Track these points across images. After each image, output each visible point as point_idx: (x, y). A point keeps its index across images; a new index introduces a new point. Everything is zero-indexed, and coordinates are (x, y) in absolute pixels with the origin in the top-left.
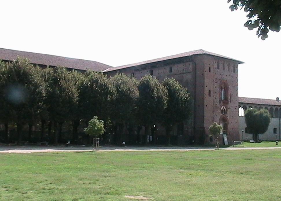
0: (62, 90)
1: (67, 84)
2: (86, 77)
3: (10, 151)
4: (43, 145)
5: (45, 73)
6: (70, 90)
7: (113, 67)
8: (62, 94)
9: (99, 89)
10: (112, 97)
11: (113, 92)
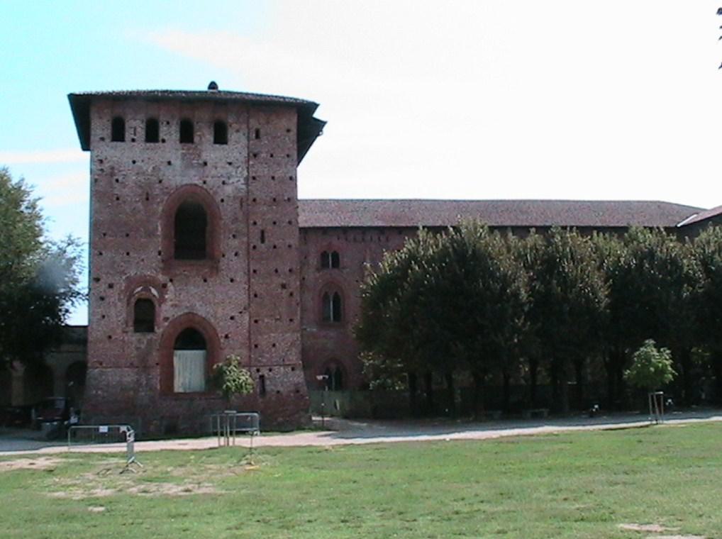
0: (567, 284)
1: (579, 268)
2: (627, 246)
3: (448, 437)
4: (537, 417)
5: (525, 247)
6: (587, 283)
7: (705, 210)
8: (569, 295)
9: (660, 274)
10: (694, 288)
11: (696, 275)
